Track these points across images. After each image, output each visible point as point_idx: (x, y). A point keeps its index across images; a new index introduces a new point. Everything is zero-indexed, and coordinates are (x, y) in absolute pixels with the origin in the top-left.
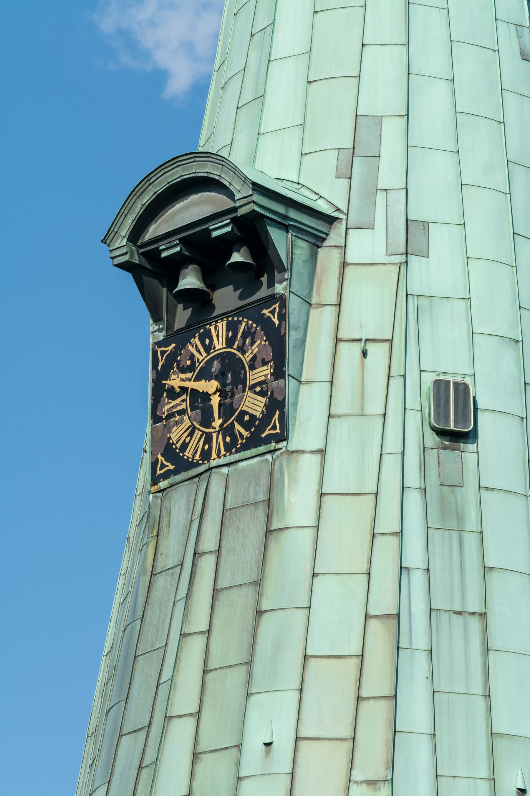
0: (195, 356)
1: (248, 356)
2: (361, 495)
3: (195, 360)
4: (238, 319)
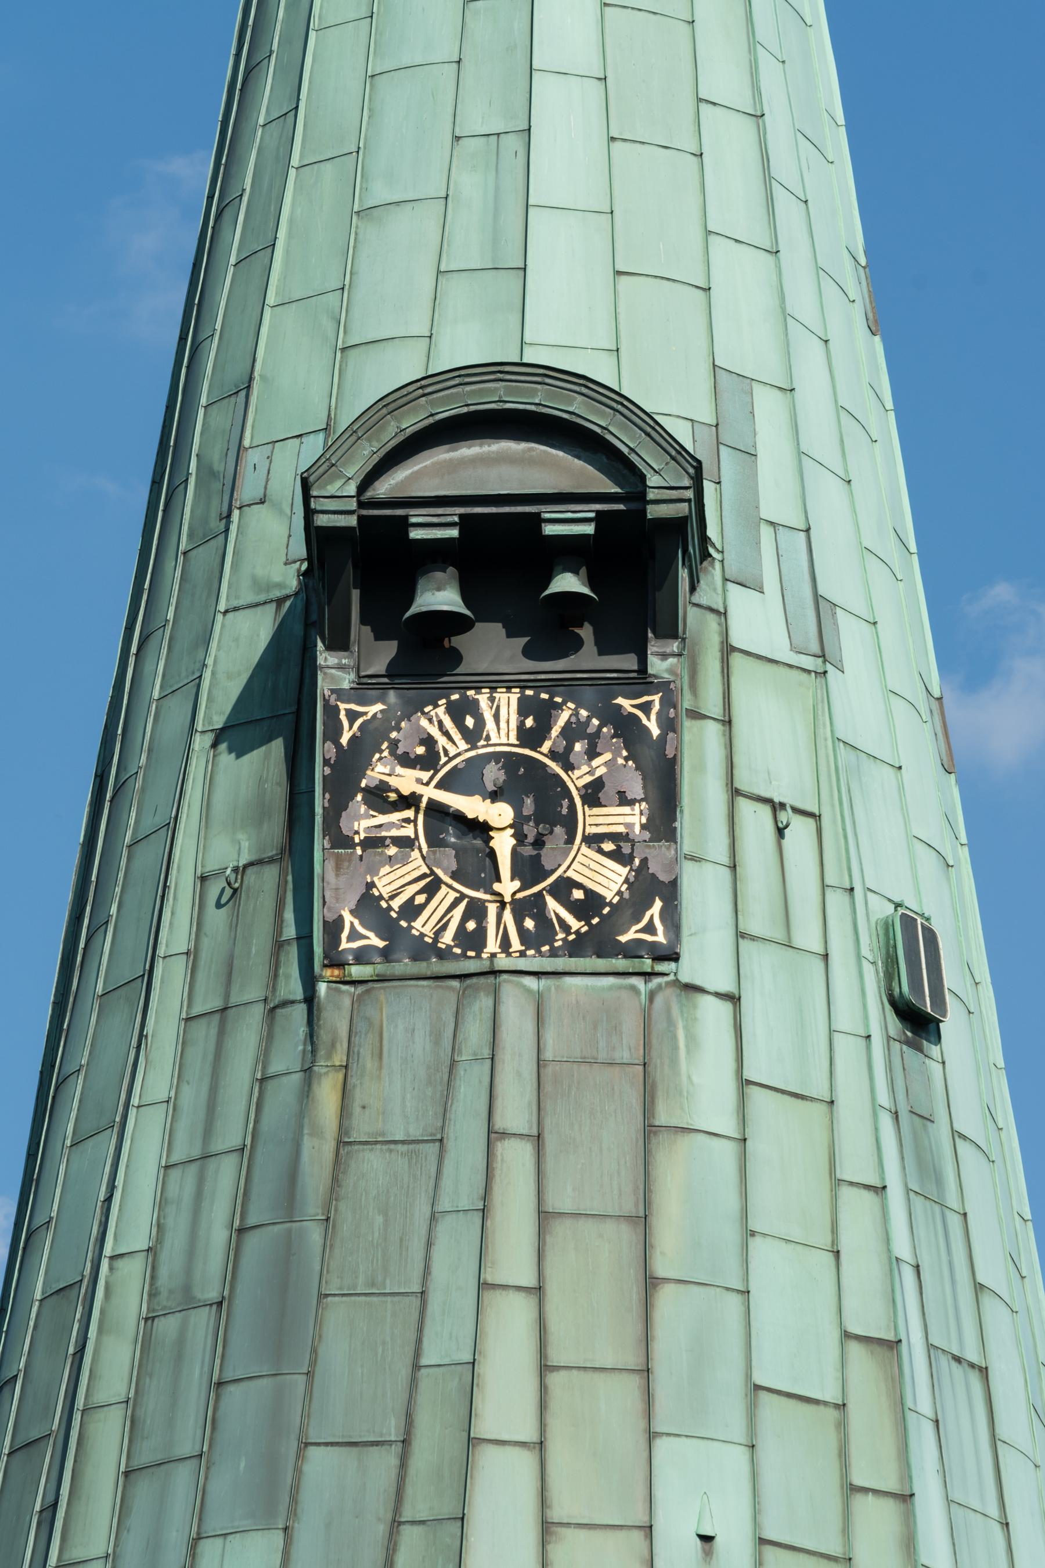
0: (436, 742)
1: (581, 777)
2: (807, 1100)
3: (436, 750)
4: (552, 697)
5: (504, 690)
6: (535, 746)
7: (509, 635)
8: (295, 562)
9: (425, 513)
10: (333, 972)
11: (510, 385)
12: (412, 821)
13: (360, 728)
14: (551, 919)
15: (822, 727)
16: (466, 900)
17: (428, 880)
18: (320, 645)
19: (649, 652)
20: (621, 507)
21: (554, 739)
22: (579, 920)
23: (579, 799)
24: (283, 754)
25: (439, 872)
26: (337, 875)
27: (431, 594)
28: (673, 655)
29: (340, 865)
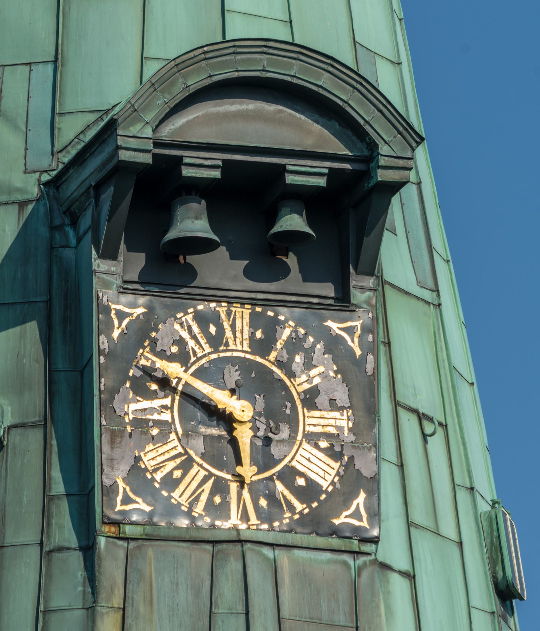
0: (187, 344)
5: (239, 305)
6: (264, 354)
7: (232, 257)
8: (34, 172)
9: (196, 155)
10: (110, 529)
11: (272, 58)
12: (169, 408)
13: (127, 326)
14: (280, 500)
15: (440, 351)
16: (213, 478)
17: (183, 458)
18: (94, 253)
19: (351, 286)
20: (348, 166)
21: (279, 350)
22: (302, 503)
23: (300, 403)
24: (38, 336)
25: (191, 452)
26: (112, 448)
27: (191, 221)
28: (370, 290)
29: (114, 439)
